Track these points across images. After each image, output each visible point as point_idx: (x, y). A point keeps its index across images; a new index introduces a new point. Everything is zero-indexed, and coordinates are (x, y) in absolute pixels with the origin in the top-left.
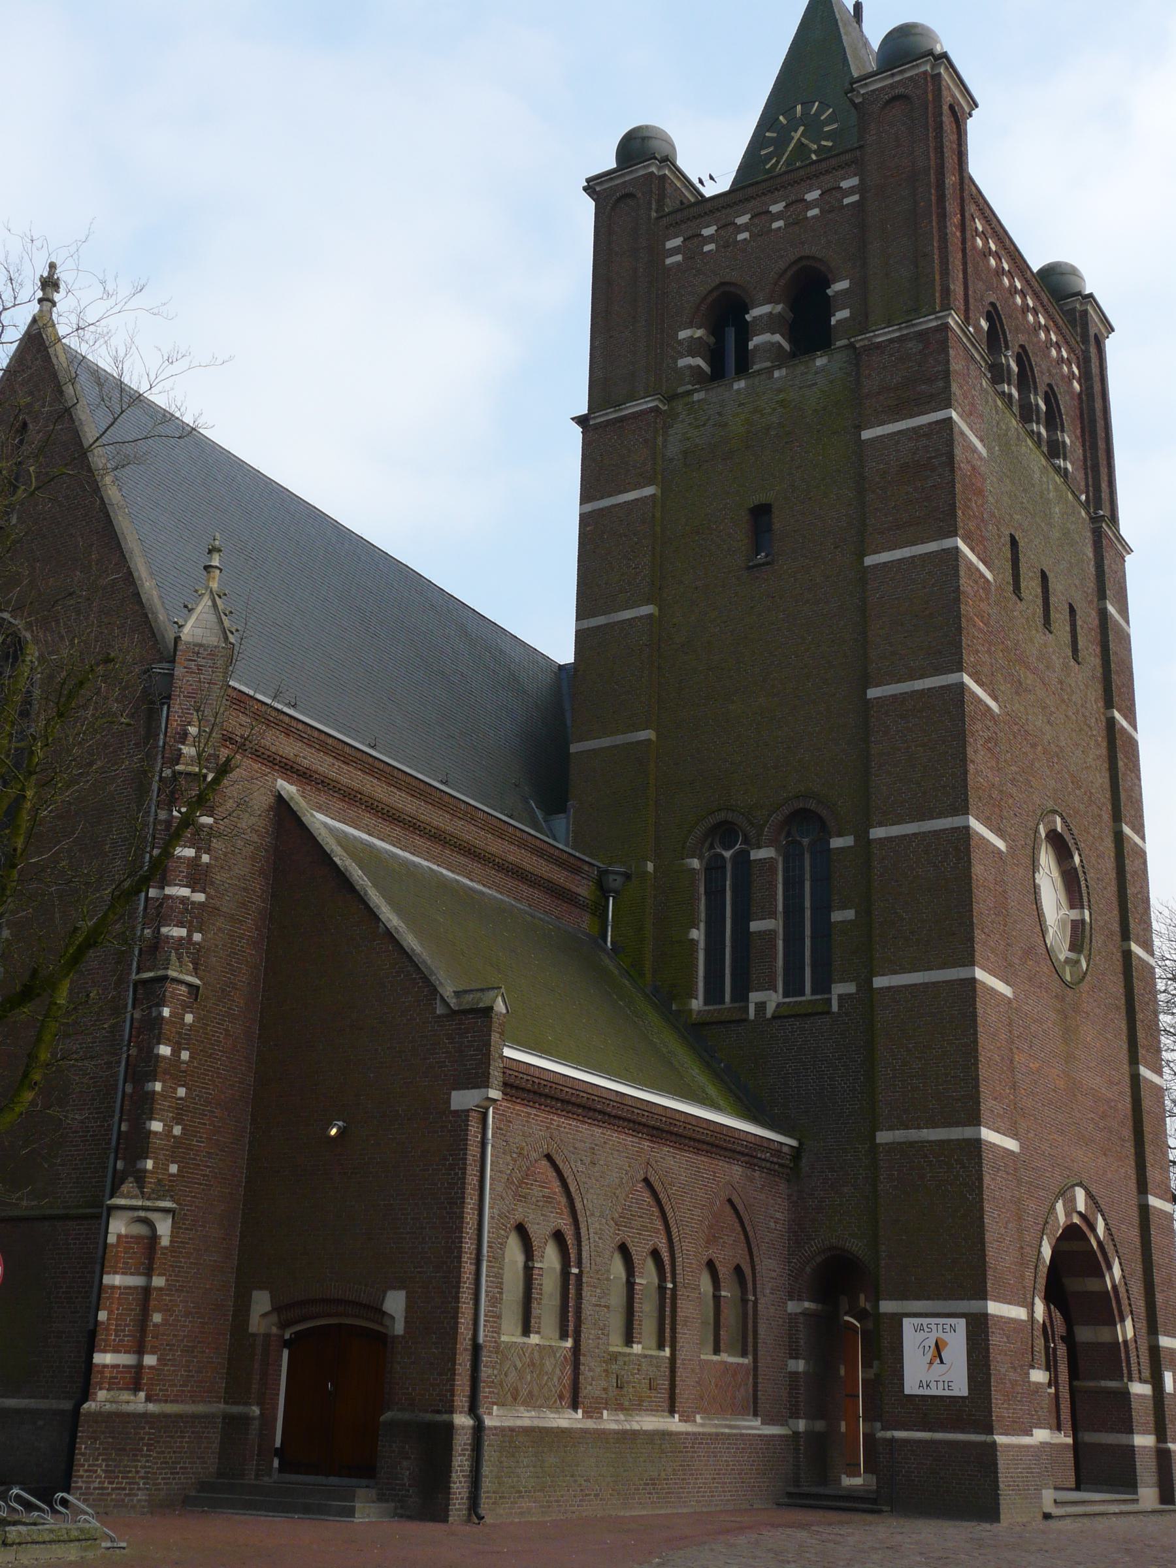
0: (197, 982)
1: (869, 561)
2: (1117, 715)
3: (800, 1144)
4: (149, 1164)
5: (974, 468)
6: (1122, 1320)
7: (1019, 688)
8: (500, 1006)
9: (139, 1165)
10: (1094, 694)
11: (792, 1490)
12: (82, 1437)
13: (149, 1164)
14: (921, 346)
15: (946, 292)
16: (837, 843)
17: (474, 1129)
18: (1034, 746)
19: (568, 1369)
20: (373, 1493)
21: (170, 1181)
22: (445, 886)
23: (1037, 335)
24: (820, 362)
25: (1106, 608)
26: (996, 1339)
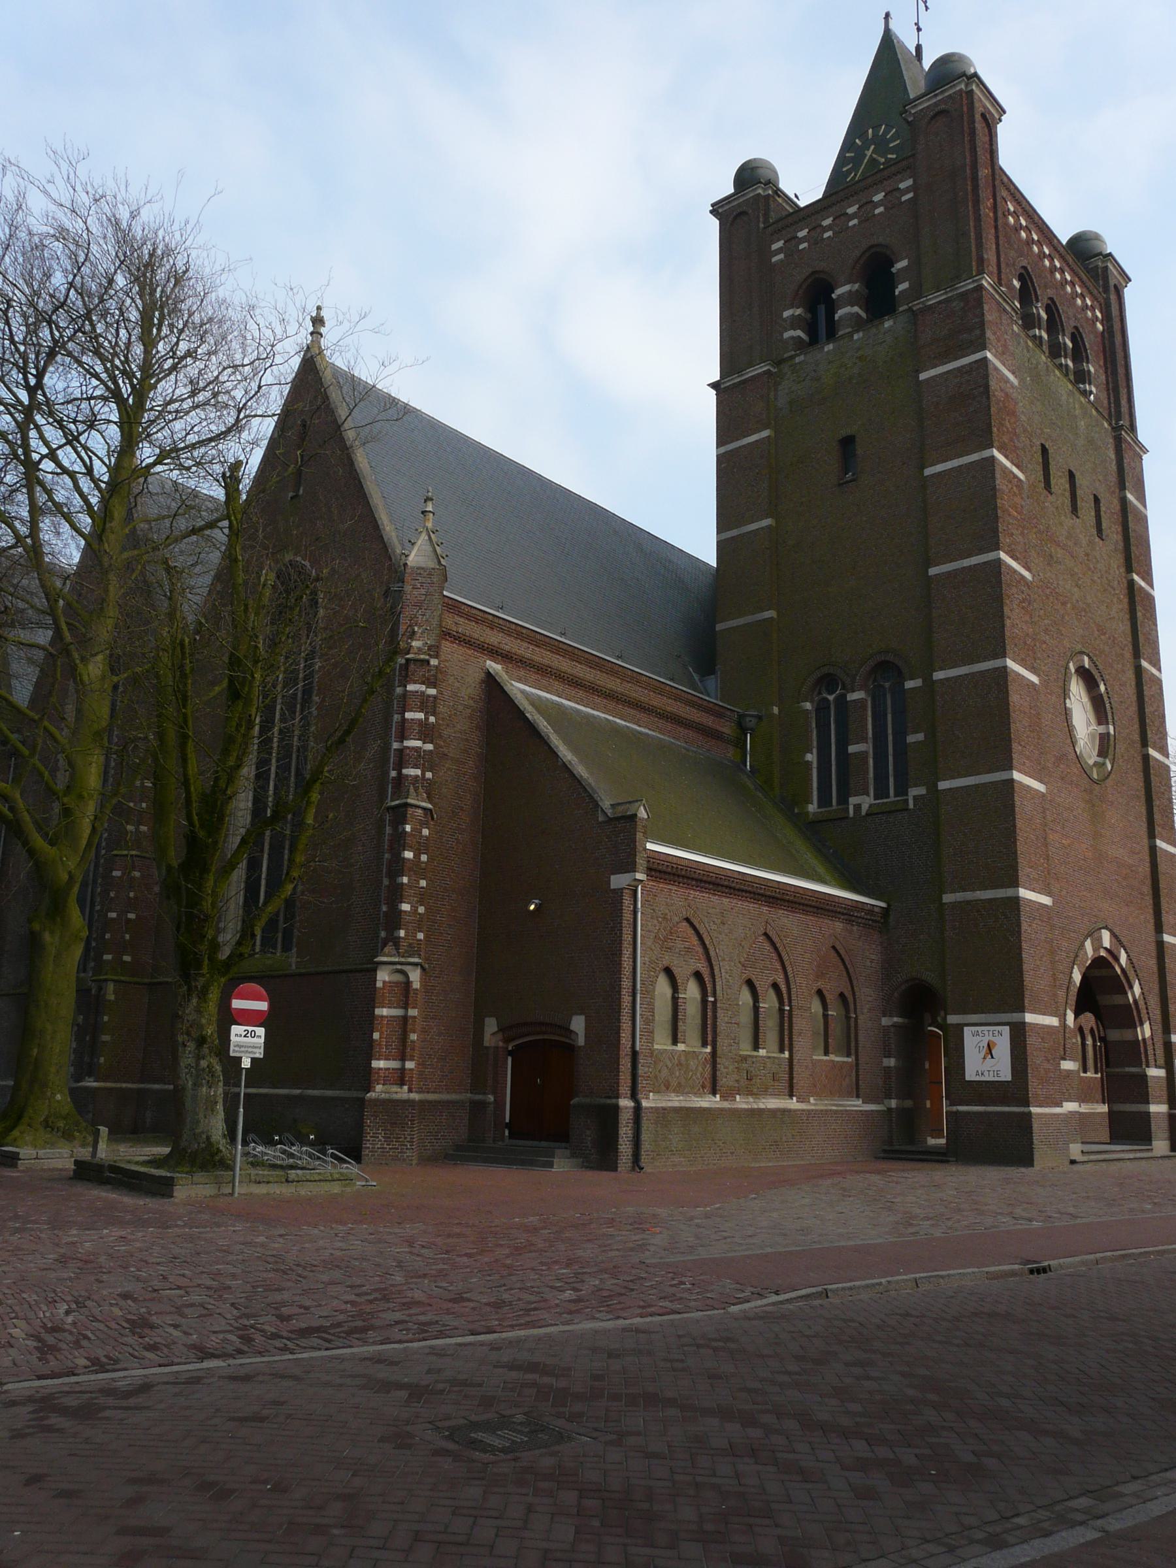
0: (430, 806)
1: (928, 472)
2: (1136, 577)
3: (889, 905)
4: (402, 933)
5: (1007, 395)
6: (1142, 1024)
7: (1050, 560)
8: (642, 813)
10: (1117, 562)
11: (886, 1147)
13: (402, 933)
14: (962, 304)
15: (981, 261)
16: (909, 684)
17: (627, 901)
18: (1064, 604)
19: (708, 1068)
20: (568, 1152)
22: (616, 730)
23: (1064, 289)
24: (887, 324)
25: (1125, 497)
26: (1032, 1040)
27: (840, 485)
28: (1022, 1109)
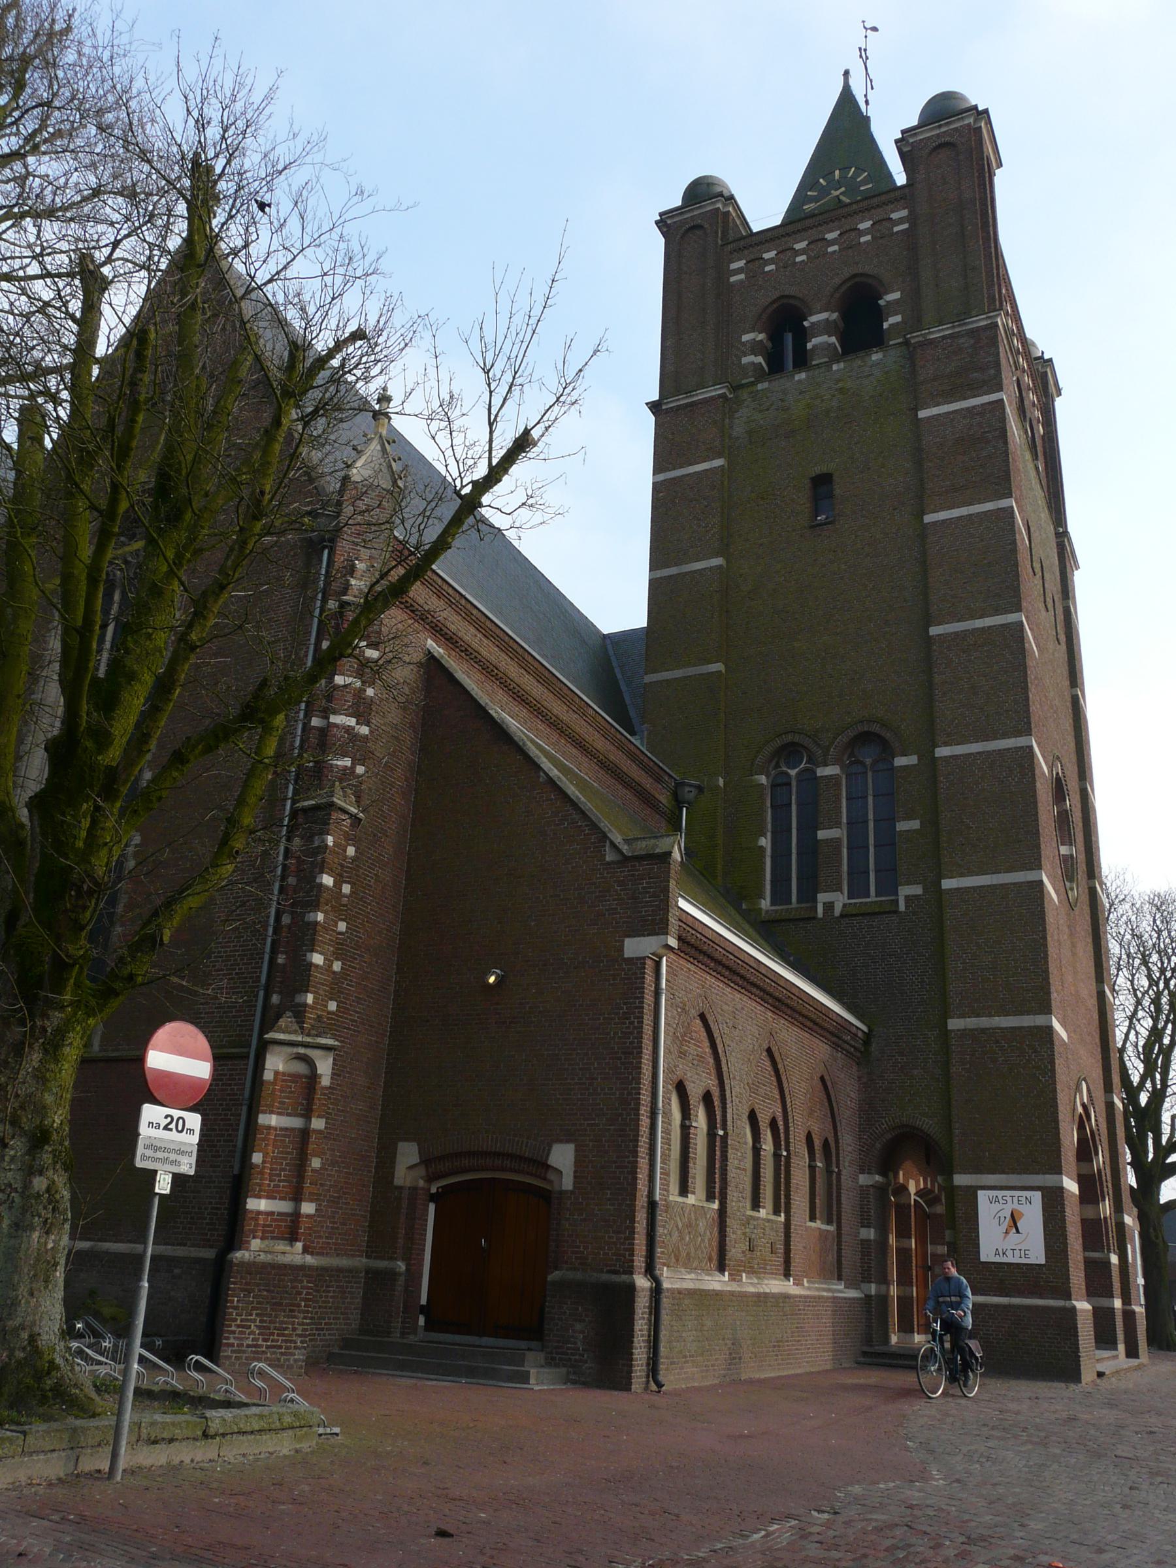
4: (310, 998)
9: (299, 999)
11: (865, 1349)
12: (234, 1290)
13: (310, 998)
14: (972, 341)
16: (900, 761)
20: (541, 1357)
21: (328, 1019)
27: (812, 527)
28: (1060, 1303)
